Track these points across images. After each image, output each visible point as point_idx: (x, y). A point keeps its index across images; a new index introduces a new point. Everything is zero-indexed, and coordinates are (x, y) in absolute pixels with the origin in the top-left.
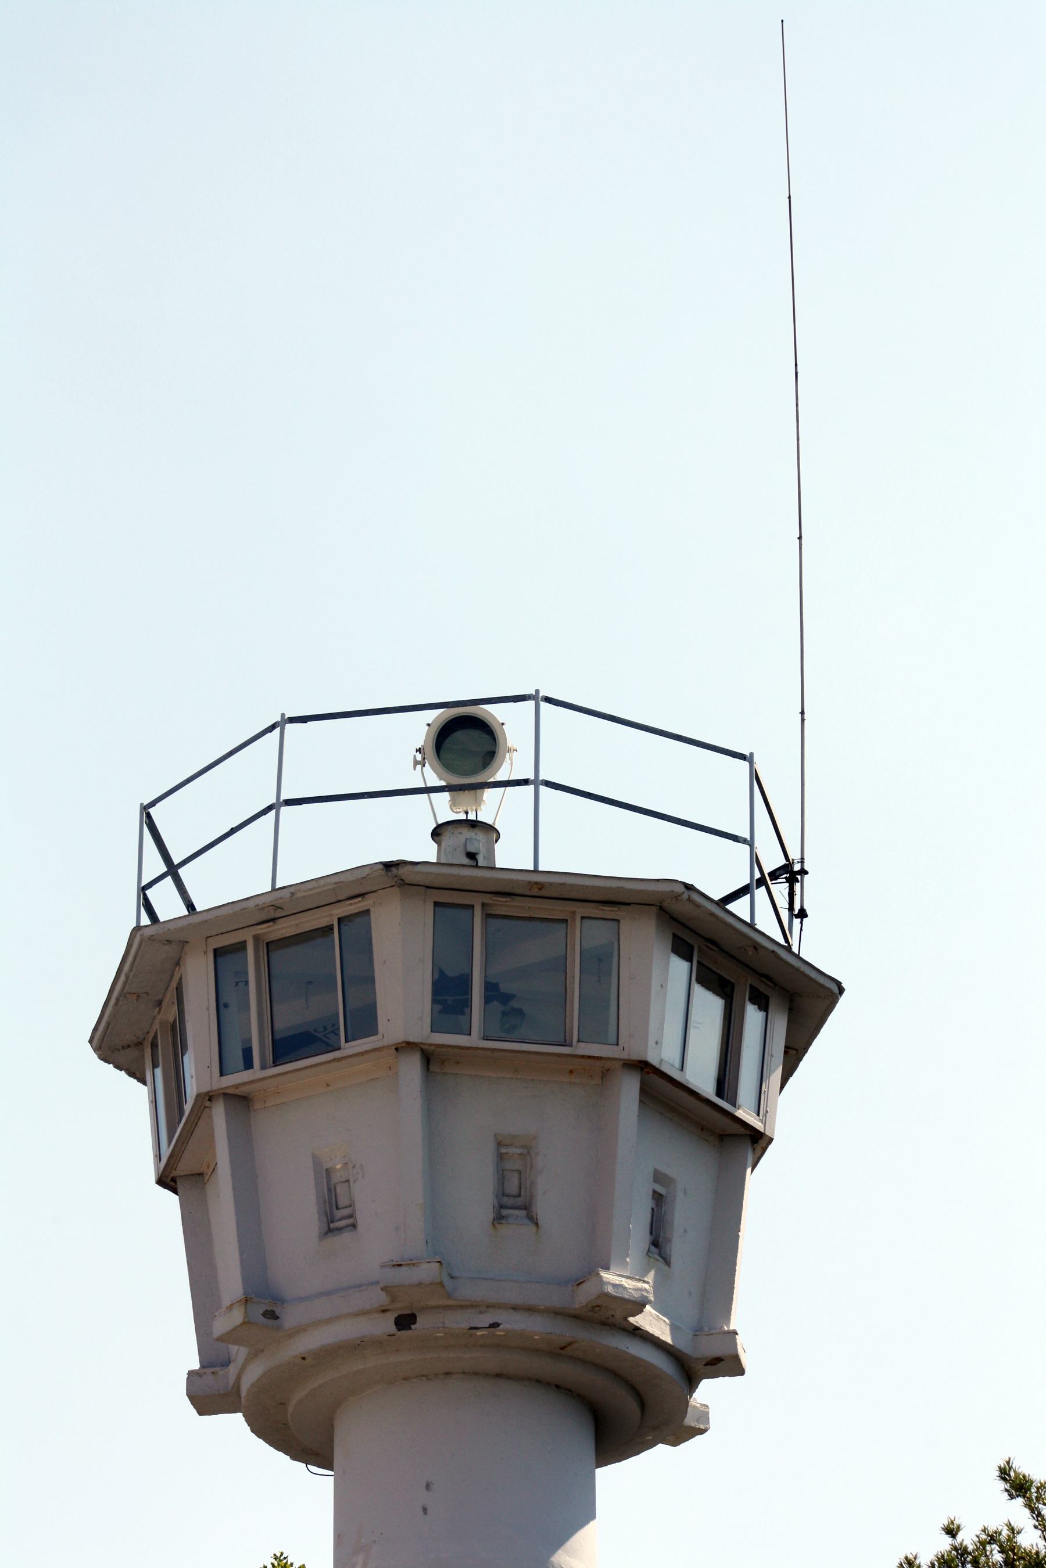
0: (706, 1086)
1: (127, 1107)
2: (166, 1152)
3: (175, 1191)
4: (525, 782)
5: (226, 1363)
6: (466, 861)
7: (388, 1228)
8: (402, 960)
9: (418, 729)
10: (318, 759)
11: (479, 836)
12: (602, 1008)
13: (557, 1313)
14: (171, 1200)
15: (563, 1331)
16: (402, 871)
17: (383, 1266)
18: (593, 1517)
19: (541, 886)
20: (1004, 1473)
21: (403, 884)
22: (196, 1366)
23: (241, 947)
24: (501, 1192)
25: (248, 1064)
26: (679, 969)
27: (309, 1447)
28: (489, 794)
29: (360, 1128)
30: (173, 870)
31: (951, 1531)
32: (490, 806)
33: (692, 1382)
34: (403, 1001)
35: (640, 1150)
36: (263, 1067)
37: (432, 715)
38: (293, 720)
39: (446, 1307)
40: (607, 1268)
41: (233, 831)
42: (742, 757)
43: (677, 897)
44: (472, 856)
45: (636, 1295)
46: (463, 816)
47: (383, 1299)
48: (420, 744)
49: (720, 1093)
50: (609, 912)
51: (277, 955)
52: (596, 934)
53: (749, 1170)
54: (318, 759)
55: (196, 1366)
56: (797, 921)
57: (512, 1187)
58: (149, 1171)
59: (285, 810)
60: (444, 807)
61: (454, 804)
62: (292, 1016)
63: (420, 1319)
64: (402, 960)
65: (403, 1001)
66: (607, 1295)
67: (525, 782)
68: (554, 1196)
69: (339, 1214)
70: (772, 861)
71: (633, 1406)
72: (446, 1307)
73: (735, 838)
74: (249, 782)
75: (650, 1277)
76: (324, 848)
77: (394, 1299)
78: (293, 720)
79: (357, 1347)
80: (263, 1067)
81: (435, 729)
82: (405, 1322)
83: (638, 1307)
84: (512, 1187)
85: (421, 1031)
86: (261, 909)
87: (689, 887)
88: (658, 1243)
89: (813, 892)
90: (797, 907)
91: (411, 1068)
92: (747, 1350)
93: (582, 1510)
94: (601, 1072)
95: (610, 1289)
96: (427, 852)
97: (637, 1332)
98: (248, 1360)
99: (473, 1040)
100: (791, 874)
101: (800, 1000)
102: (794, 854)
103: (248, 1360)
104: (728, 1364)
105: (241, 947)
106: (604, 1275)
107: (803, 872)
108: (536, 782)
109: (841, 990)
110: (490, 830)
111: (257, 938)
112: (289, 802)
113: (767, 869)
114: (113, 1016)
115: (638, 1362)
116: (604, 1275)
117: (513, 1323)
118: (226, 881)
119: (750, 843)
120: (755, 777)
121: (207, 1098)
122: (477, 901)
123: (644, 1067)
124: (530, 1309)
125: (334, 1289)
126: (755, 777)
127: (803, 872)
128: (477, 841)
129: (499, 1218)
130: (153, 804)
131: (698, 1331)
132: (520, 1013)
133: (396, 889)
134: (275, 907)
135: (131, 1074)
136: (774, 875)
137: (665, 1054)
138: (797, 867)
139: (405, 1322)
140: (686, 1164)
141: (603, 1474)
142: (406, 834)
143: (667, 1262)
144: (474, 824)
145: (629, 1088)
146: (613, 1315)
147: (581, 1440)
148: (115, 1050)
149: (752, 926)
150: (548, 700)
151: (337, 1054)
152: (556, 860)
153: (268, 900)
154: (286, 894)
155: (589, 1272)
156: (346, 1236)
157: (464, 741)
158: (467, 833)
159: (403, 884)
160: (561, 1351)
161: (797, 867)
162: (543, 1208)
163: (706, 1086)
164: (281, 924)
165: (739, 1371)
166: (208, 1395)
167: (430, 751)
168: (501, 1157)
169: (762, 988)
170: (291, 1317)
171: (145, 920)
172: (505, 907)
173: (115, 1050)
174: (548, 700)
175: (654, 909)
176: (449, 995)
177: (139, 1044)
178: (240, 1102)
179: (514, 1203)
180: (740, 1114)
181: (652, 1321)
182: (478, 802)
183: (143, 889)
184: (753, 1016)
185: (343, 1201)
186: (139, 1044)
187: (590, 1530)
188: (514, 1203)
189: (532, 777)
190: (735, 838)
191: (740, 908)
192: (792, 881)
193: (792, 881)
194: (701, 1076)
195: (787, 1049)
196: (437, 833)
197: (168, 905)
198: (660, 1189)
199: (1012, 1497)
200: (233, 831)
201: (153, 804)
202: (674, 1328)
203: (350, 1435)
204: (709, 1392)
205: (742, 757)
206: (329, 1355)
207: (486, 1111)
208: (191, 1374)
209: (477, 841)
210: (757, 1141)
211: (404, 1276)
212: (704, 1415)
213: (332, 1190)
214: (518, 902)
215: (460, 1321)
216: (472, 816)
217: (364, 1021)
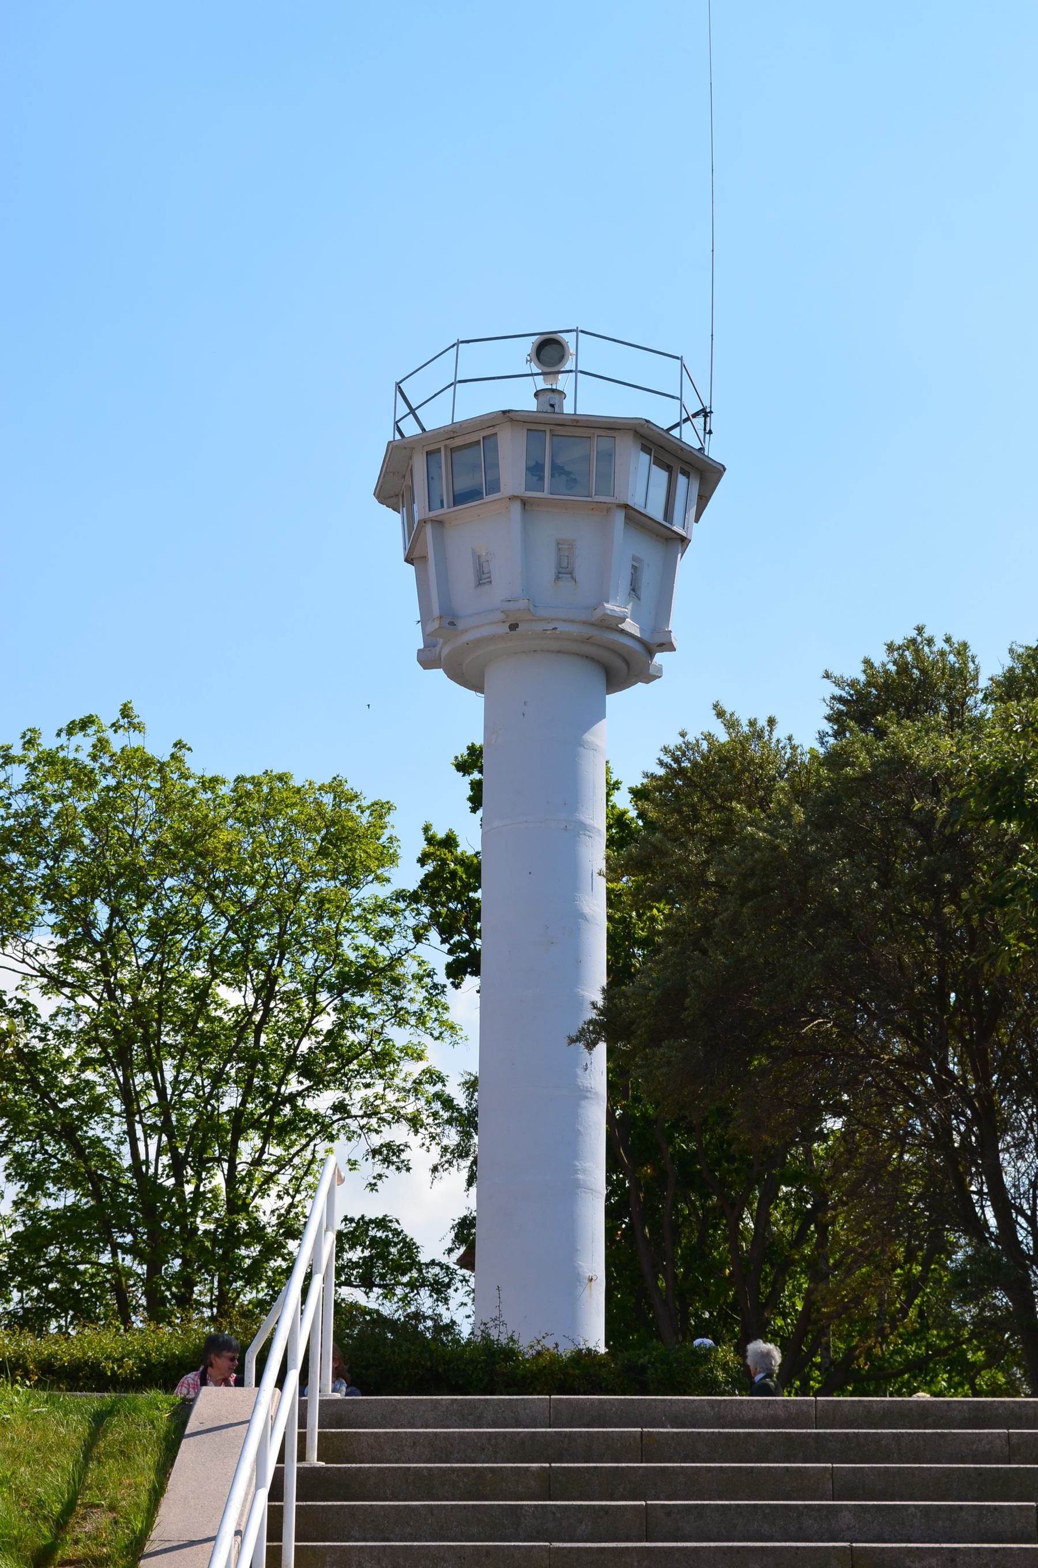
0: (658, 515)
2: (408, 547)
4: (571, 371)
5: (434, 646)
6: (550, 409)
7: (506, 583)
8: (512, 458)
9: (528, 345)
10: (475, 360)
11: (556, 396)
12: (607, 478)
19: (577, 421)
20: (715, 706)
21: (512, 420)
22: (422, 647)
23: (438, 450)
24: (559, 566)
25: (442, 506)
26: (645, 458)
27: (476, 685)
28: (560, 376)
29: (492, 535)
30: (412, 411)
31: (683, 735)
32: (564, 383)
33: (651, 654)
34: (512, 475)
35: (625, 545)
36: (449, 507)
38: (462, 342)
39: (531, 620)
40: (608, 602)
41: (436, 395)
42: (677, 358)
43: (642, 426)
44: (552, 406)
45: (621, 614)
47: (502, 616)
49: (665, 519)
50: (611, 433)
52: (605, 444)
54: (475, 360)
55: (422, 647)
56: (707, 436)
57: (564, 564)
58: (402, 556)
60: (541, 383)
61: (545, 380)
62: (463, 484)
64: (512, 458)
65: (512, 475)
66: (607, 615)
67: (571, 371)
68: (583, 569)
70: (694, 407)
71: (623, 666)
72: (531, 620)
73: (673, 397)
74: (442, 373)
75: (630, 607)
77: (507, 617)
78: (462, 342)
79: (492, 638)
80: (449, 507)
81: (536, 345)
82: (513, 627)
83: (623, 620)
84: (564, 564)
85: (521, 491)
88: (634, 590)
89: (714, 421)
90: (708, 429)
91: (516, 508)
92: (676, 639)
93: (600, 714)
94: (607, 509)
95: (609, 612)
96: (530, 405)
97: (623, 631)
98: (444, 644)
99: (545, 494)
100: (705, 413)
101: (705, 474)
102: (707, 404)
103: (444, 644)
104: (668, 646)
105: (438, 450)
107: (711, 412)
111: (446, 446)
112: (460, 382)
114: (383, 482)
117: (563, 627)
119: (681, 400)
120: (683, 365)
121: (424, 522)
122: (547, 428)
123: (626, 507)
124: (572, 621)
125: (481, 611)
126: (683, 365)
127: (711, 412)
129: (558, 578)
130: (401, 382)
131: (653, 631)
132: (575, 481)
134: (453, 431)
136: (695, 415)
137: (636, 501)
138: (708, 410)
139: (513, 627)
140: (648, 551)
142: (522, 397)
143: (639, 599)
144: (553, 391)
146: (612, 624)
149: (680, 440)
150: (582, 332)
151: (482, 501)
153: (450, 428)
154: (458, 425)
157: (549, 350)
158: (550, 395)
159: (512, 420)
160: (587, 640)
162: (579, 574)
163: (658, 515)
165: (672, 648)
166: (427, 660)
167: (534, 356)
168: (559, 549)
169: (686, 468)
170: (461, 625)
171: (398, 437)
172: (560, 431)
174: (582, 332)
175: (632, 432)
176: (535, 470)
178: (439, 523)
179: (565, 571)
180: (675, 528)
181: (630, 626)
182: (557, 379)
183: (396, 423)
184: (682, 480)
185: (486, 571)
187: (602, 726)
188: (565, 571)
190: (673, 397)
191: (675, 433)
192: (706, 416)
193: (706, 416)
194: (656, 511)
195: (700, 497)
196: (536, 395)
197: (410, 428)
198: (636, 564)
199: (468, 748)
200: (436, 395)
201: (401, 382)
202: (641, 630)
204: (660, 658)
205: (677, 358)
206: (479, 642)
207: (550, 529)
210: (684, 541)
212: (660, 669)
213: (481, 565)
214: (568, 429)
215: (539, 627)
216: (554, 387)
217: (494, 486)
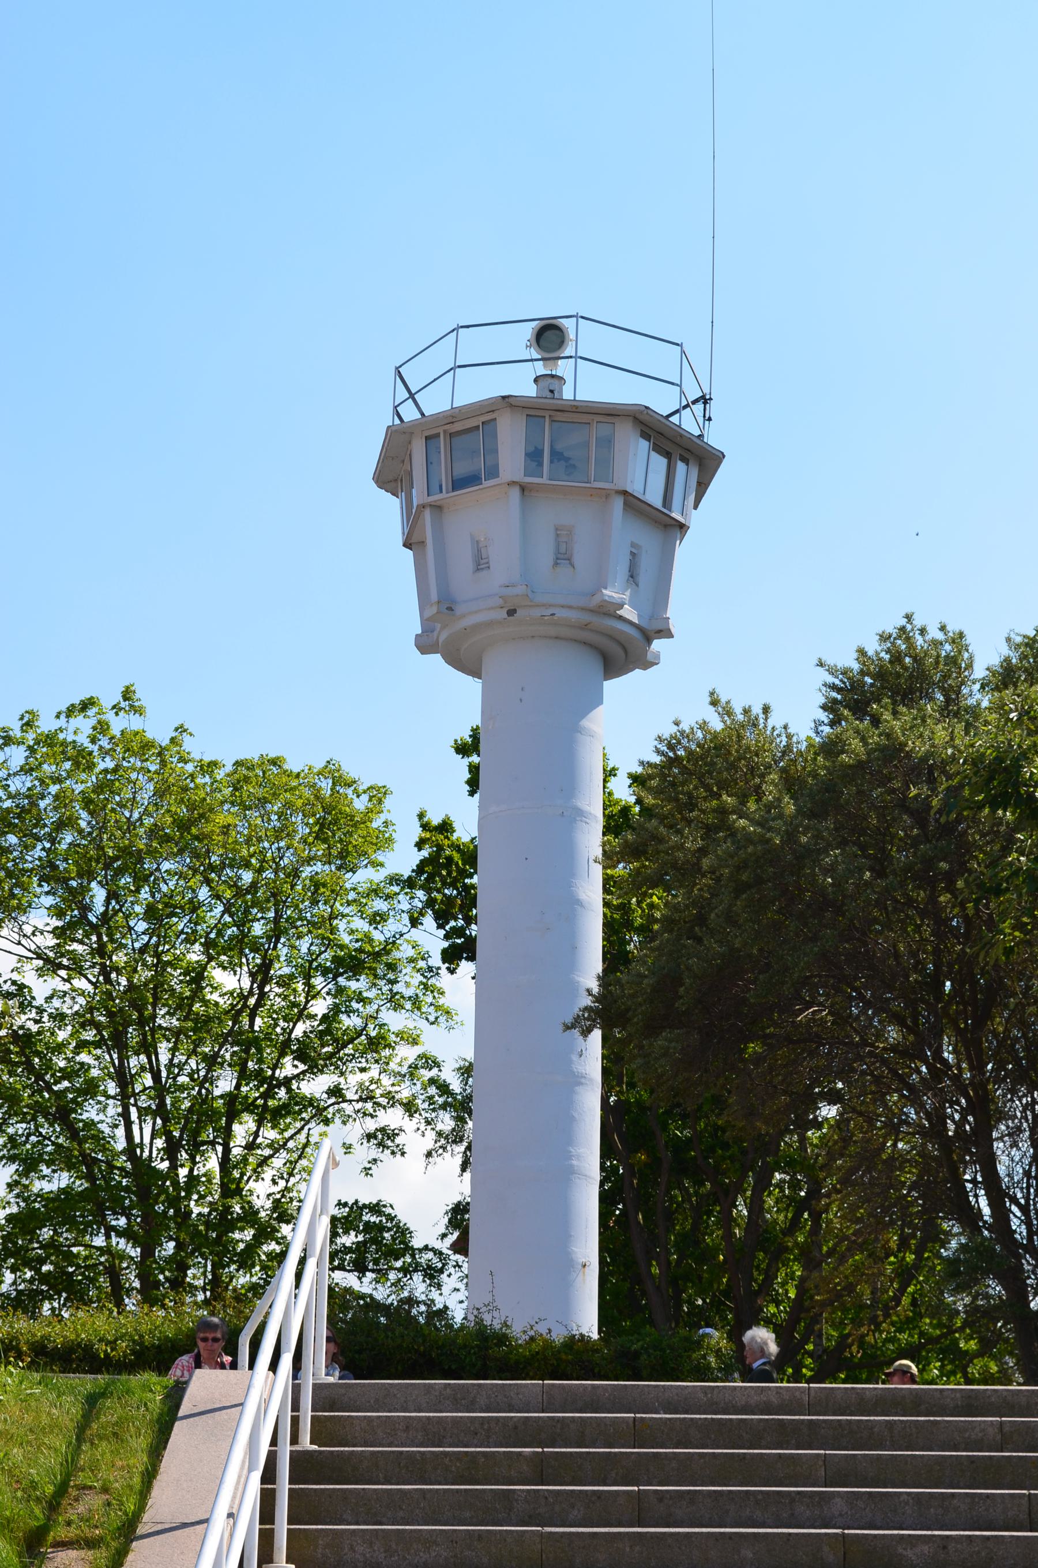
0: (657, 501)
1: (389, 509)
3: (411, 549)
4: (571, 357)
5: (432, 631)
6: (549, 395)
9: (528, 331)
10: (475, 346)
11: (556, 381)
12: (606, 465)
13: (583, 609)
14: (409, 553)
15: (586, 617)
16: (510, 400)
17: (501, 586)
18: (602, 703)
19: (577, 407)
20: (712, 694)
21: (511, 406)
22: (419, 632)
23: (438, 435)
24: (558, 552)
25: (441, 492)
26: (644, 445)
28: (560, 362)
29: (490, 520)
32: (563, 368)
33: (649, 641)
34: (511, 460)
35: (623, 532)
36: (447, 493)
37: (534, 324)
38: (462, 327)
40: (606, 588)
41: (435, 380)
42: (678, 345)
43: (641, 412)
44: (552, 391)
45: (619, 601)
46: (549, 372)
47: (501, 602)
48: (529, 337)
49: (664, 506)
51: (455, 440)
53: (678, 542)
54: (475, 346)
55: (419, 632)
56: (707, 422)
57: (563, 549)
58: (399, 540)
59: (458, 370)
60: (541, 369)
61: (545, 366)
62: (462, 469)
63: (518, 611)
65: (511, 460)
67: (571, 357)
69: (482, 562)
70: (694, 394)
73: (673, 384)
74: (442, 357)
75: (628, 593)
76: (476, 389)
78: (462, 327)
79: (490, 624)
80: (447, 493)
82: (511, 612)
83: (621, 606)
85: (519, 476)
86: (446, 417)
87: (647, 408)
88: (633, 576)
89: (714, 409)
90: (707, 416)
91: (516, 492)
92: (674, 626)
93: (597, 700)
94: (606, 495)
95: (607, 598)
96: (530, 390)
97: (620, 617)
98: (442, 629)
99: (544, 480)
100: (705, 400)
101: (704, 461)
103: (442, 629)
104: (665, 633)
105: (438, 435)
106: (604, 591)
107: (711, 399)
108: (576, 357)
109: (724, 456)
110: (561, 378)
111: (445, 431)
112: (459, 367)
113: (691, 399)
115: (622, 632)
116: (604, 591)
117: (561, 613)
118: (436, 402)
119: (680, 386)
120: (683, 352)
121: (422, 507)
122: (547, 414)
123: (625, 493)
124: (570, 607)
125: (479, 597)
126: (683, 352)
127: (711, 399)
128: (554, 384)
129: (556, 564)
131: (651, 618)
132: (574, 466)
133: (508, 409)
134: (453, 416)
135: (393, 494)
136: (694, 402)
137: (635, 487)
139: (511, 612)
140: (647, 538)
141: (608, 685)
142: (521, 383)
143: (637, 585)
144: (553, 376)
145: (618, 503)
146: (609, 610)
147: (598, 667)
148: (384, 483)
149: (679, 426)
150: (582, 317)
151: (481, 487)
152: (583, 396)
153: (449, 413)
154: (457, 410)
155: (596, 591)
156: (485, 572)
157: (549, 336)
158: (550, 380)
159: (511, 406)
160: (585, 627)
161: (708, 397)
162: (577, 559)
163: (657, 501)
164: (456, 425)
166: (425, 645)
168: (558, 535)
170: (459, 610)
171: (397, 421)
172: (560, 416)
173: (384, 483)
174: (582, 317)
176: (534, 456)
177: (396, 480)
178: (437, 508)
179: (563, 557)
180: (673, 515)
181: (628, 612)
182: (556, 365)
184: (681, 467)
186: (396, 480)
187: (600, 710)
188: (563, 557)
189: (573, 354)
190: (673, 384)
191: (675, 419)
192: (705, 403)
193: (705, 403)
194: (655, 498)
195: (699, 483)
196: (536, 380)
197: (410, 413)
198: (634, 551)
200: (435, 380)
202: (639, 616)
203: (487, 666)
205: (678, 345)
207: (549, 515)
208: (417, 635)
209: (554, 384)
210: (682, 528)
211: (510, 591)
212: (657, 656)
213: (479, 551)
214: (566, 415)
215: (537, 613)
216: (554, 373)
217: (493, 472)
